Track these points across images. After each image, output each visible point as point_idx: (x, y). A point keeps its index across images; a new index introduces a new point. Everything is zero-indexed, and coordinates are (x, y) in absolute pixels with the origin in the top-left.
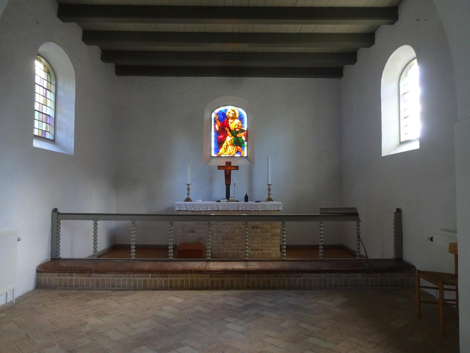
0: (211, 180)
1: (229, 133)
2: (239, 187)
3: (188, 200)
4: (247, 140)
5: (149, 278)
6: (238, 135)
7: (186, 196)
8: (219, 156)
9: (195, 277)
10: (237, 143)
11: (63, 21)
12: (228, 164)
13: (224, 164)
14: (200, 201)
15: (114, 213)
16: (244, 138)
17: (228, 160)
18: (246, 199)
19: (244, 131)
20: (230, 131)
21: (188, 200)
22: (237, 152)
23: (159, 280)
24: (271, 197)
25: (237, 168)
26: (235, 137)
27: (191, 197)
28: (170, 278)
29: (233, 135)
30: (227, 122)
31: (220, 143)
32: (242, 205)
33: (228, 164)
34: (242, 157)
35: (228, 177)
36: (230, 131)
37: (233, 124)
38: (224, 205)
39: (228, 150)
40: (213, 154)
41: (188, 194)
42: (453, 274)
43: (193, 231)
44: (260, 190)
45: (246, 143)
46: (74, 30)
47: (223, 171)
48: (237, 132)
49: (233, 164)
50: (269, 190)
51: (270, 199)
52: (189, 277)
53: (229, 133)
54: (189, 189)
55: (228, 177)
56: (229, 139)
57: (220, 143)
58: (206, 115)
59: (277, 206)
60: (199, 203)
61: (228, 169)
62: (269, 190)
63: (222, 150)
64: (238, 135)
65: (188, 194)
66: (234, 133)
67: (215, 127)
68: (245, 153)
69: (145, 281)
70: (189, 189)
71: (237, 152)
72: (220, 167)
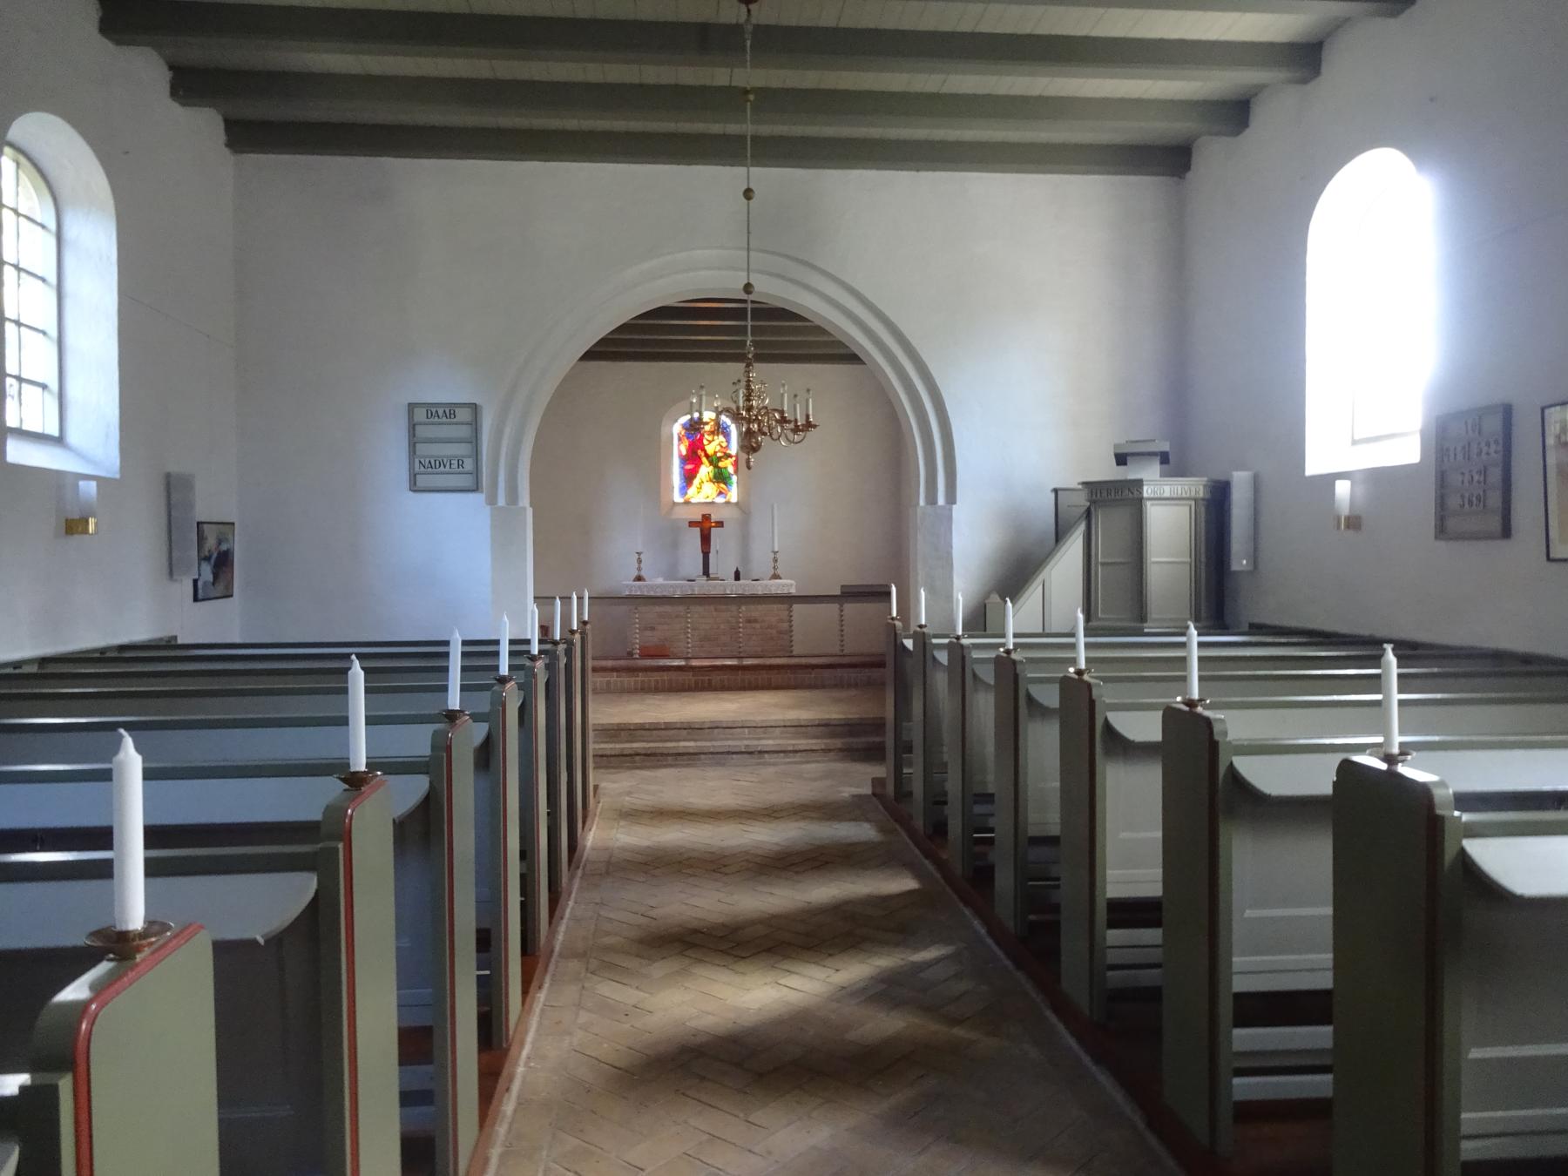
0: (675, 545)
1: (704, 459)
2: (725, 559)
3: (639, 578)
4: (736, 472)
5: (614, 678)
6: (721, 464)
7: (635, 573)
8: (687, 503)
9: (674, 675)
10: (720, 478)
11: (118, 43)
12: (706, 517)
13: (699, 518)
14: (660, 581)
15: (238, 640)
16: (731, 469)
17: (706, 512)
18: (737, 576)
19: (730, 456)
20: (707, 456)
21: (639, 578)
22: (720, 493)
23: (628, 680)
24: (779, 572)
25: (720, 524)
26: (716, 466)
27: (643, 573)
28: (641, 677)
29: (711, 463)
30: (701, 440)
31: (689, 477)
32: (732, 588)
33: (706, 517)
34: (728, 503)
35: (706, 539)
36: (707, 456)
37: (713, 446)
38: (702, 587)
39: (704, 491)
40: (678, 498)
41: (639, 569)
42: (1061, 689)
43: (653, 629)
44: (760, 561)
45: (734, 478)
46: (145, 70)
47: (697, 530)
48: (719, 459)
49: (714, 518)
50: (776, 560)
51: (776, 577)
52: (666, 676)
53: (704, 459)
54: (640, 561)
55: (706, 539)
56: (705, 470)
57: (689, 477)
58: (664, 431)
59: (787, 585)
60: (657, 582)
61: (705, 527)
62: (776, 560)
63: (692, 491)
64: (721, 464)
65: (639, 569)
66: (714, 461)
67: (679, 449)
68: (733, 495)
69: (608, 683)
70: (640, 561)
71: (720, 493)
72: (692, 524)
